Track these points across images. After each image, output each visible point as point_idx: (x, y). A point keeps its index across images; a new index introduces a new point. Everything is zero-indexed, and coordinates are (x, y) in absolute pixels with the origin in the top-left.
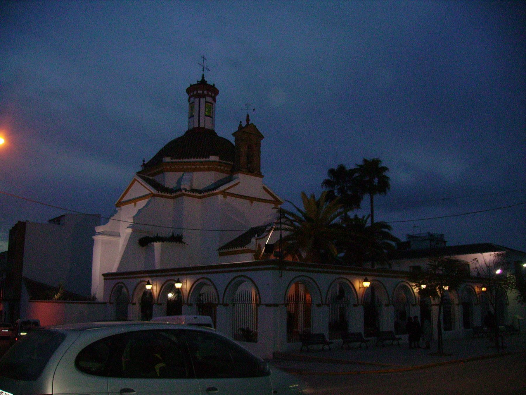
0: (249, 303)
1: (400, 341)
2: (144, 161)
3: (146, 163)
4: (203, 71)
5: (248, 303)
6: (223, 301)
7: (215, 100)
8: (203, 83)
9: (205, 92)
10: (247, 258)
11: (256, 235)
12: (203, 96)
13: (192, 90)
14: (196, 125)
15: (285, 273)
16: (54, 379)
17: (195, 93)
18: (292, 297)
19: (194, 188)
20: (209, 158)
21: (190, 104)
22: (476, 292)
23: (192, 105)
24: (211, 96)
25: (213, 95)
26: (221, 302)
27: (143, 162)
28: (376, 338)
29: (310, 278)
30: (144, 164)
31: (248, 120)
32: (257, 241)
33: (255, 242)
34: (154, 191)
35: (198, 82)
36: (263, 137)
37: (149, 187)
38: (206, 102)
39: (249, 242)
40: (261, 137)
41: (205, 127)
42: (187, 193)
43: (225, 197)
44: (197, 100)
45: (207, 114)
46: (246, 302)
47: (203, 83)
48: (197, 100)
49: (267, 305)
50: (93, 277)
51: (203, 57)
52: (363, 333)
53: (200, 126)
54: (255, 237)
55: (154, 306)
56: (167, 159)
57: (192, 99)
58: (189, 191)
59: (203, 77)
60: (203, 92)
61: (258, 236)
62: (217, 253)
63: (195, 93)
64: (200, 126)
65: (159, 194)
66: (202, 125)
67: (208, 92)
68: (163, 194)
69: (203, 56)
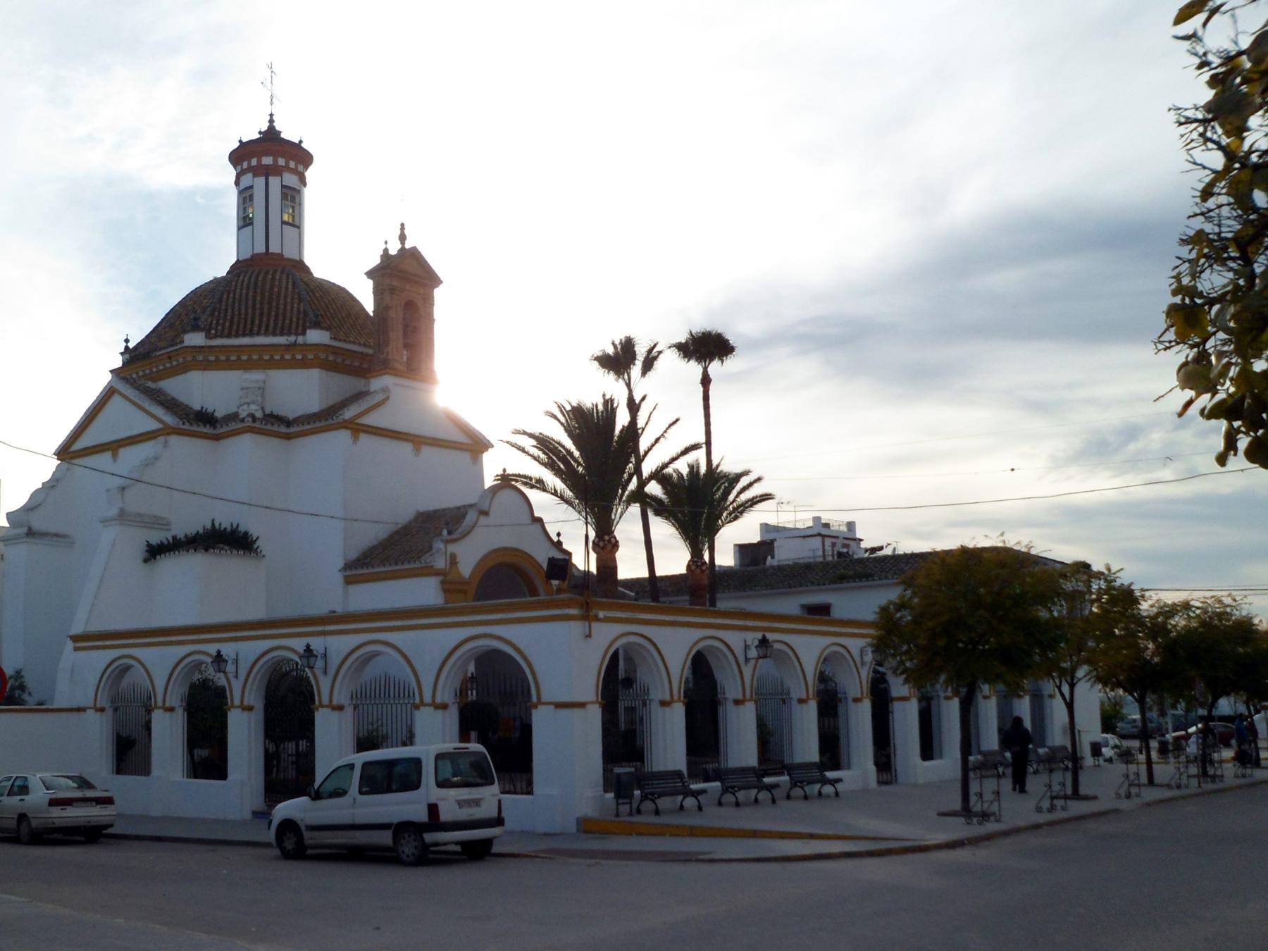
0: (382, 702)
1: (839, 786)
2: (127, 341)
3: (131, 345)
4: (272, 103)
5: (370, 704)
6: (242, 701)
8: (271, 137)
9: (281, 162)
11: (445, 532)
13: (243, 156)
14: (260, 249)
15: (596, 626)
17: (254, 162)
18: (361, 691)
20: (304, 333)
21: (240, 193)
23: (245, 197)
26: (428, 699)
27: (125, 344)
28: (718, 784)
29: (642, 636)
30: (127, 348)
31: (402, 238)
33: (444, 549)
34: (169, 419)
35: (260, 133)
37: (159, 412)
38: (283, 187)
42: (257, 425)
44: (261, 180)
45: (286, 218)
46: (392, 702)
47: (271, 137)
48: (261, 180)
49: (560, 706)
51: (1170, 110)
52: (685, 771)
53: (270, 251)
54: (440, 534)
55: (230, 714)
56: (195, 339)
57: (247, 180)
58: (261, 420)
59: (271, 121)
61: (450, 533)
64: (270, 251)
65: (184, 427)
66: (275, 248)
67: (287, 163)
68: (195, 428)
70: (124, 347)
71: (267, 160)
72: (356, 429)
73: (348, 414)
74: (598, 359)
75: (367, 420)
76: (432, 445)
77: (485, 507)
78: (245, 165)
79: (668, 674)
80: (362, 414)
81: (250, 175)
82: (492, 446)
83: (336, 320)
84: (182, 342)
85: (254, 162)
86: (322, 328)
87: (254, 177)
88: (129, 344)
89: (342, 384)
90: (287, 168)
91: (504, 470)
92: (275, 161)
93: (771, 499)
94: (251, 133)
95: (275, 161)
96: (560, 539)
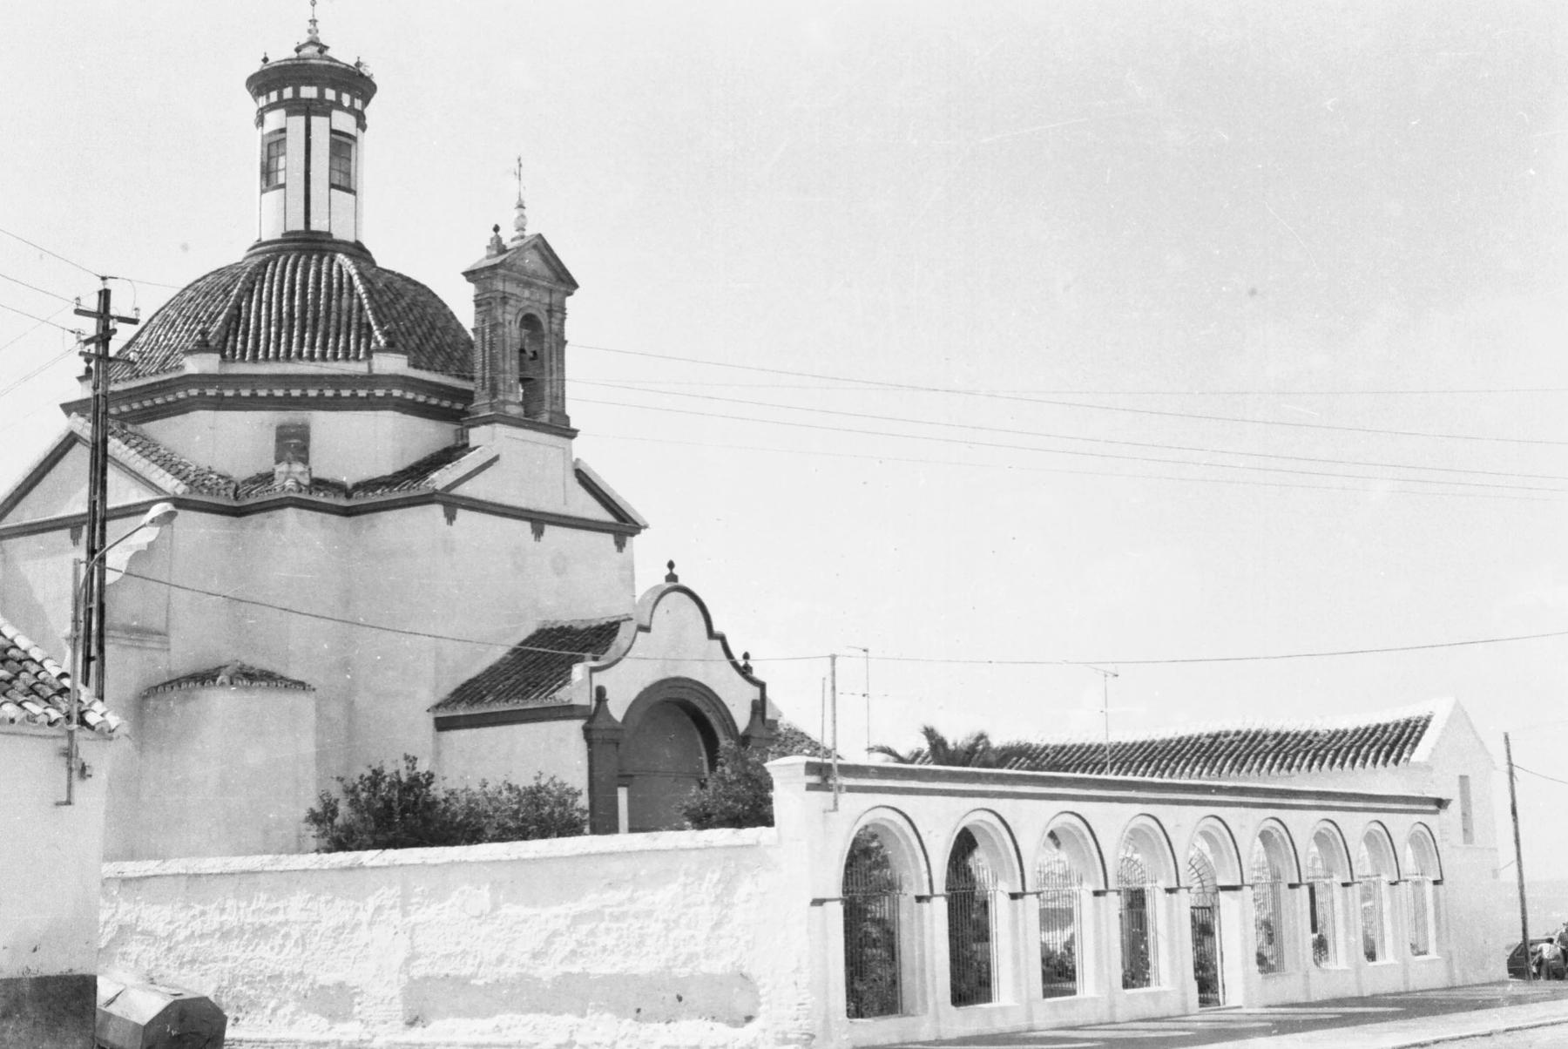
10: (1292, 752)
16: (1520, 926)
19: (78, 444)
24: (351, 110)
25: (358, 104)
32: (264, 195)
36: (576, 286)
38: (333, 131)
39: (564, 677)
42: (304, 496)
48: (299, 121)
62: (429, 720)
67: (339, 96)
70: (84, 370)
71: (309, 92)
72: (452, 503)
73: (440, 479)
74: (466, 274)
75: (465, 490)
77: (646, 623)
78: (274, 96)
80: (121, 466)
81: (281, 113)
82: (646, 527)
83: (414, 337)
84: (182, 367)
85: (288, 93)
86: (397, 351)
87: (288, 114)
89: (427, 435)
90: (338, 105)
91: (265, 60)
92: (321, 93)
93: (1425, 727)
94: (282, 52)
95: (321, 93)
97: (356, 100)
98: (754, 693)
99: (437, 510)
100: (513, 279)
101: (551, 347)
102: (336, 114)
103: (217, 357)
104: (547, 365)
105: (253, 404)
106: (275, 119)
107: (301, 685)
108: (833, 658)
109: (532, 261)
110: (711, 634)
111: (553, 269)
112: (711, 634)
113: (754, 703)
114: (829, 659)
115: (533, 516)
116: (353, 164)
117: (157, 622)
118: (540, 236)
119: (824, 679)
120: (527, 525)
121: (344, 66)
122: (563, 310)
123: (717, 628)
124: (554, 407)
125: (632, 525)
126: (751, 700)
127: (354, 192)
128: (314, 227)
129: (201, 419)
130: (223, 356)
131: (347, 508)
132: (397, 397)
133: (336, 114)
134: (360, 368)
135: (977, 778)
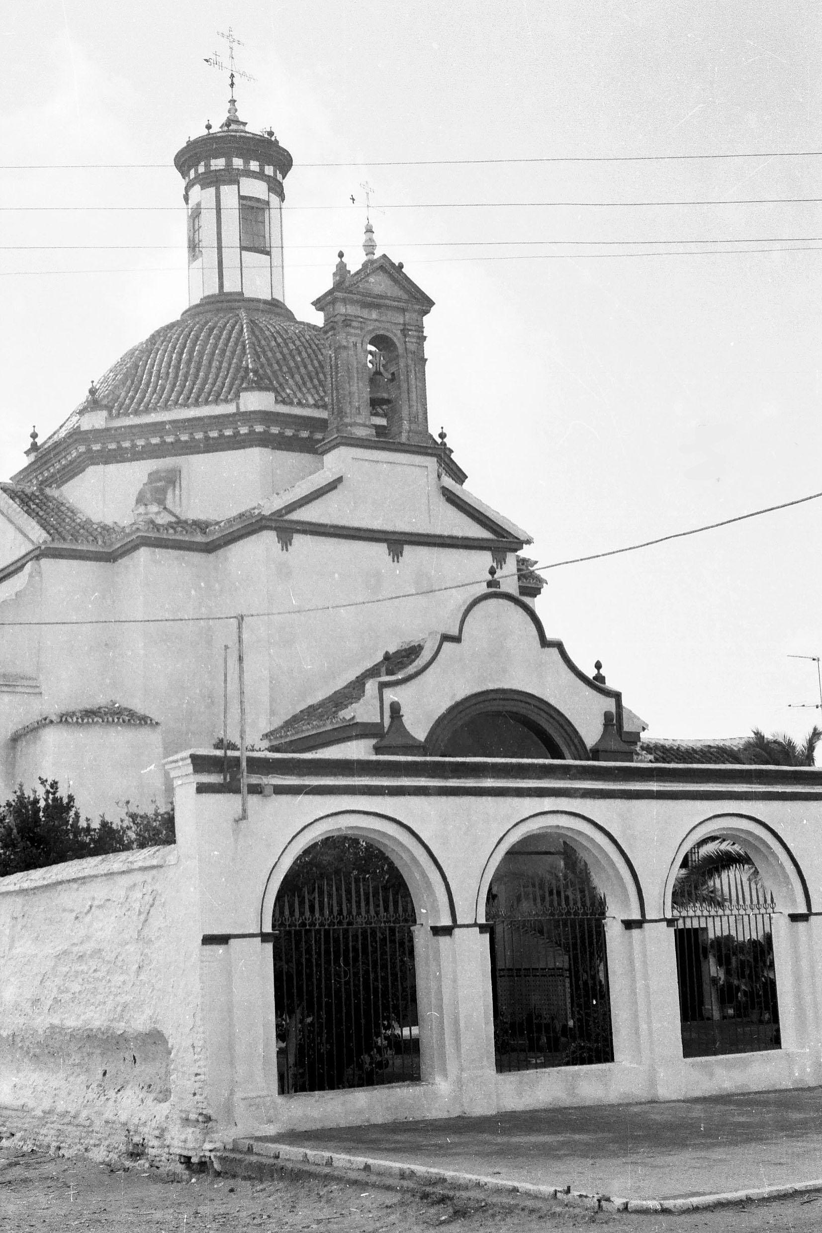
2: (34, 436)
7: (277, 189)
12: (230, 177)
22: (492, 540)
24: (260, 175)
25: (269, 170)
27: (32, 440)
30: (34, 447)
31: (370, 247)
36: (431, 303)
38: (242, 198)
40: (425, 303)
41: (242, 294)
43: (285, 541)
50: (419, 1014)
59: (233, 109)
60: (229, 164)
63: (201, 169)
66: (230, 286)
69: (227, 33)
71: (218, 163)
76: (305, 532)
79: (444, 878)
88: (36, 440)
95: (229, 164)
96: (601, 671)
97: (266, 167)
98: (609, 704)
99: (269, 538)
100: (353, 302)
101: (407, 366)
102: (243, 181)
103: (105, 413)
104: (404, 386)
105: (137, 455)
106: (202, 195)
107: (143, 721)
108: (241, 618)
109: (379, 284)
110: (545, 642)
111: (407, 292)
112: (545, 642)
113: (607, 716)
114: (234, 622)
115: (390, 537)
116: (267, 228)
117: (28, 668)
118: (384, 256)
119: (226, 647)
120: (382, 548)
121: (251, 135)
122: (420, 328)
123: (550, 635)
124: (413, 426)
125: (511, 540)
126: (603, 712)
127: (268, 253)
128: (226, 289)
129: (94, 474)
130: (110, 414)
131: (207, 544)
132: (260, 433)
133: (243, 181)
134: (231, 409)
135: (566, 772)
